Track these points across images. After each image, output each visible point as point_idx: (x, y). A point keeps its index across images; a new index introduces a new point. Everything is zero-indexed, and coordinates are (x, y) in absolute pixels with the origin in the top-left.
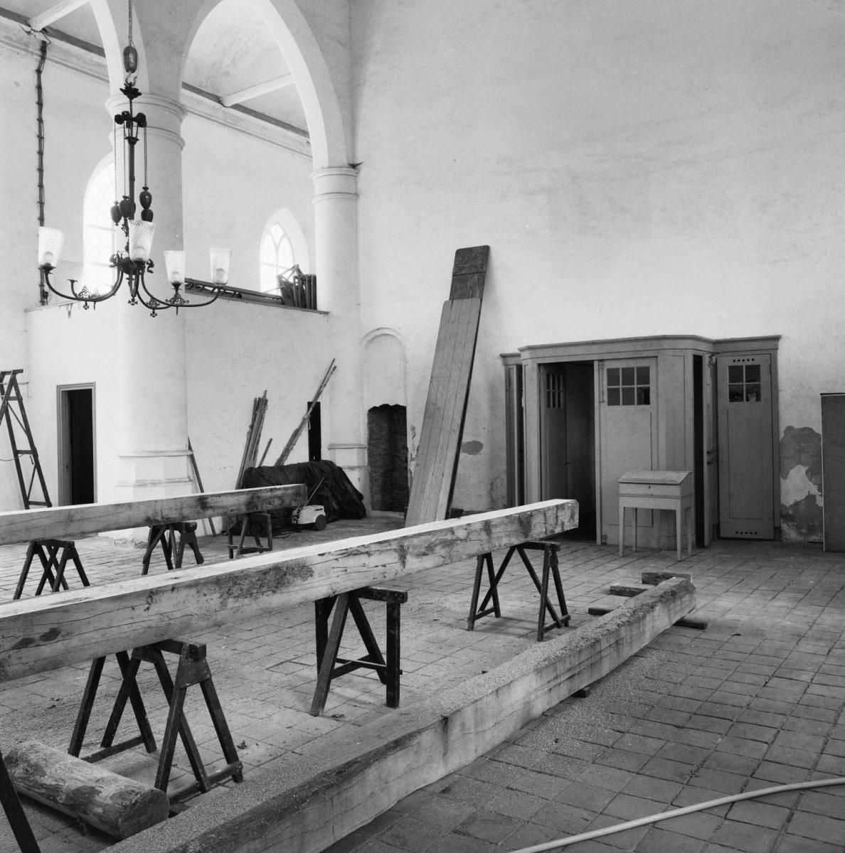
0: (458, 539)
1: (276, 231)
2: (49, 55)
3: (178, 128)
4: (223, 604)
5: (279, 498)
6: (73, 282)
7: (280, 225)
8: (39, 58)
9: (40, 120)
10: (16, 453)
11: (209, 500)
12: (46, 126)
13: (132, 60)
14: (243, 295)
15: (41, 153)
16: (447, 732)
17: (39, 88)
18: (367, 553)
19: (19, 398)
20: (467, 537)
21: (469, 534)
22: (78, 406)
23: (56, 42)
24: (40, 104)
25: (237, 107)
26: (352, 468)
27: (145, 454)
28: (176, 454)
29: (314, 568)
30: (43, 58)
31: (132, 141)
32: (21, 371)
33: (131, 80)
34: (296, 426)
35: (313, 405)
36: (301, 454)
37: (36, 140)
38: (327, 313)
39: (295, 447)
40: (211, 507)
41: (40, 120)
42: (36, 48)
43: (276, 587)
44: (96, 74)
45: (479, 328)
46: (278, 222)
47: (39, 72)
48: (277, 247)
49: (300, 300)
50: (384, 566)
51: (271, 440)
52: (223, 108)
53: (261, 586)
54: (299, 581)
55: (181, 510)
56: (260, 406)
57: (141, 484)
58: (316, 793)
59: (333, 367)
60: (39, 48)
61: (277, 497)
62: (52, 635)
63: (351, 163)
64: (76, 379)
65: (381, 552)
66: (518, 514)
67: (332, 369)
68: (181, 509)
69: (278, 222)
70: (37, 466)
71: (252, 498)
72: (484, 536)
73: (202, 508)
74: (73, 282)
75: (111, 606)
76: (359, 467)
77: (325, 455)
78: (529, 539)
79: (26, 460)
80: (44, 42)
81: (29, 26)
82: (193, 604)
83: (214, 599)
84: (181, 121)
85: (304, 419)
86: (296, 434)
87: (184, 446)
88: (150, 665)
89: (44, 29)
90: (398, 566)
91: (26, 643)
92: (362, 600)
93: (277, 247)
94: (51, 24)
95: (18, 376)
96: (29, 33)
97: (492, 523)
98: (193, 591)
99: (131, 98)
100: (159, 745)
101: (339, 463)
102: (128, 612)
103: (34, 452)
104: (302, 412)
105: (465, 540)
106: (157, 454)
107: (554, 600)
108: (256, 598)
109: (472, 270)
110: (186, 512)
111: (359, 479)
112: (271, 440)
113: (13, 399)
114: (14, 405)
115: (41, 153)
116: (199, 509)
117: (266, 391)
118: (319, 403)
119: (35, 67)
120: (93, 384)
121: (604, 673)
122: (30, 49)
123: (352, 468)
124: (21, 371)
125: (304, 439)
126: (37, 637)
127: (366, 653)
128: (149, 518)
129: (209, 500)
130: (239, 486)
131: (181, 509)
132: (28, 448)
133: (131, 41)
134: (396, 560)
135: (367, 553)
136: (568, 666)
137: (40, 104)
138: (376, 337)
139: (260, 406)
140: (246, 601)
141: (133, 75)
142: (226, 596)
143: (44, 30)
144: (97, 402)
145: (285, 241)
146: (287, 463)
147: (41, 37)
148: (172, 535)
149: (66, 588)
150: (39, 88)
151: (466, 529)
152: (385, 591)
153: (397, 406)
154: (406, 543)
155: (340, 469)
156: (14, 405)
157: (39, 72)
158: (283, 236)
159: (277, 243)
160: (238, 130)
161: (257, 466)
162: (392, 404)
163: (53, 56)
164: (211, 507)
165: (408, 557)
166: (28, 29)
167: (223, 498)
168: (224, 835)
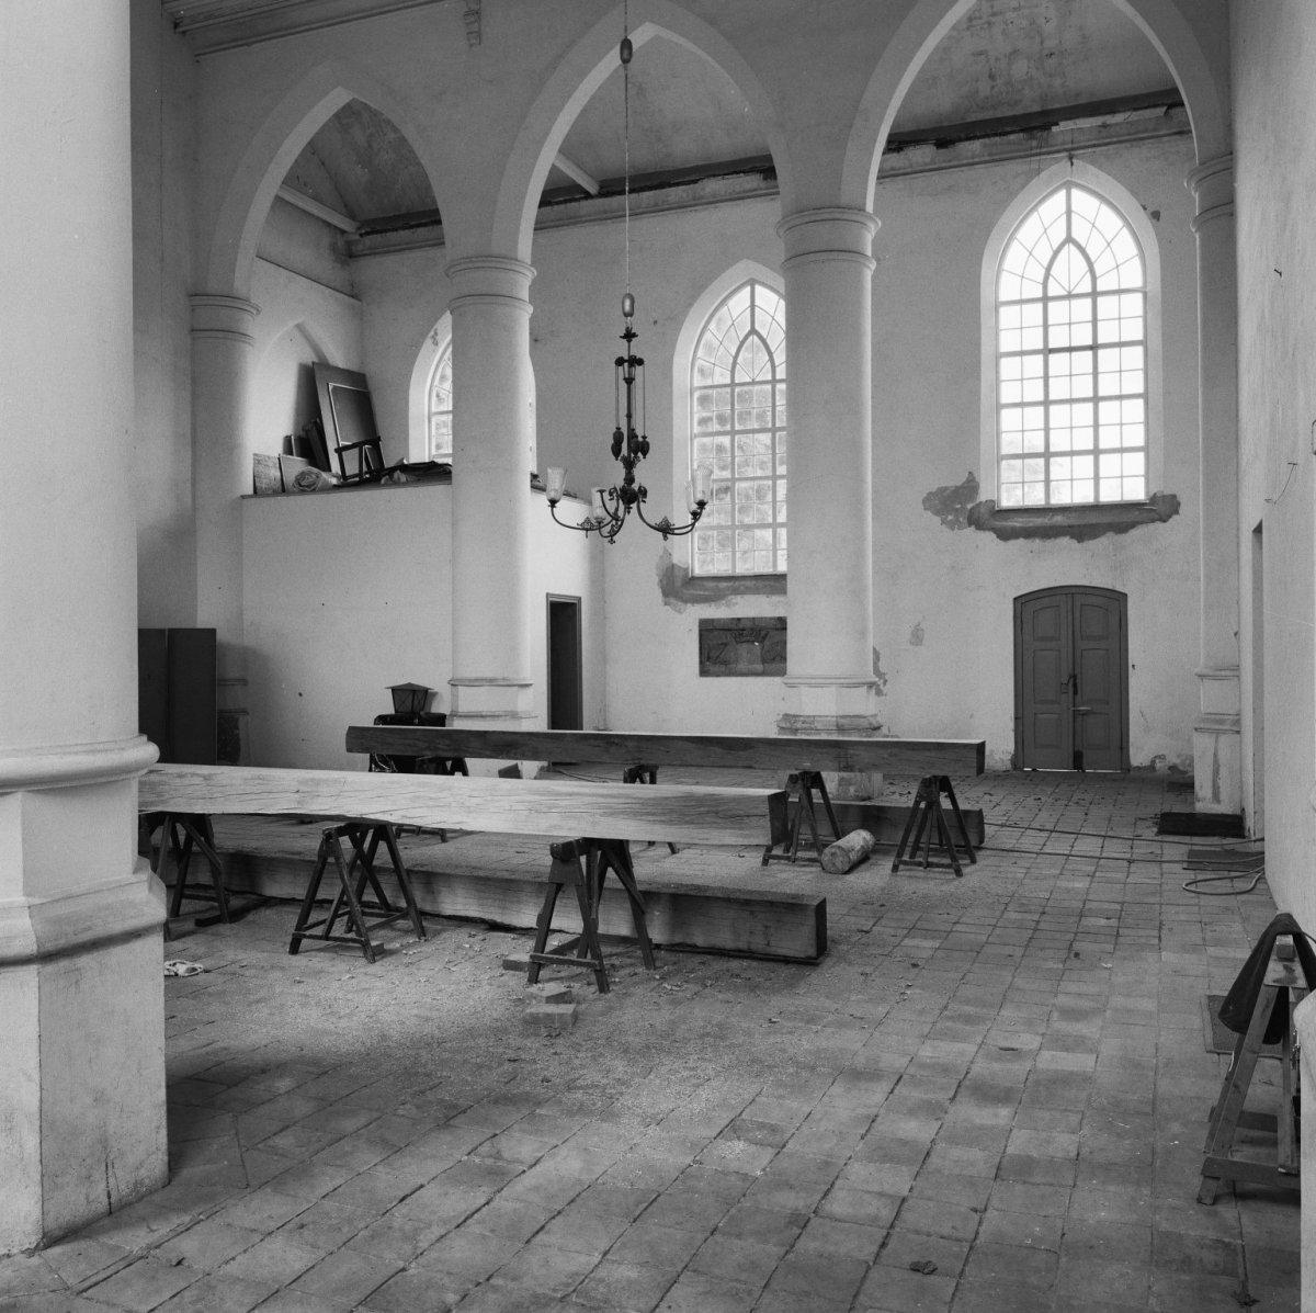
31: (629, 381)
99: (629, 341)
130: (221, 712)
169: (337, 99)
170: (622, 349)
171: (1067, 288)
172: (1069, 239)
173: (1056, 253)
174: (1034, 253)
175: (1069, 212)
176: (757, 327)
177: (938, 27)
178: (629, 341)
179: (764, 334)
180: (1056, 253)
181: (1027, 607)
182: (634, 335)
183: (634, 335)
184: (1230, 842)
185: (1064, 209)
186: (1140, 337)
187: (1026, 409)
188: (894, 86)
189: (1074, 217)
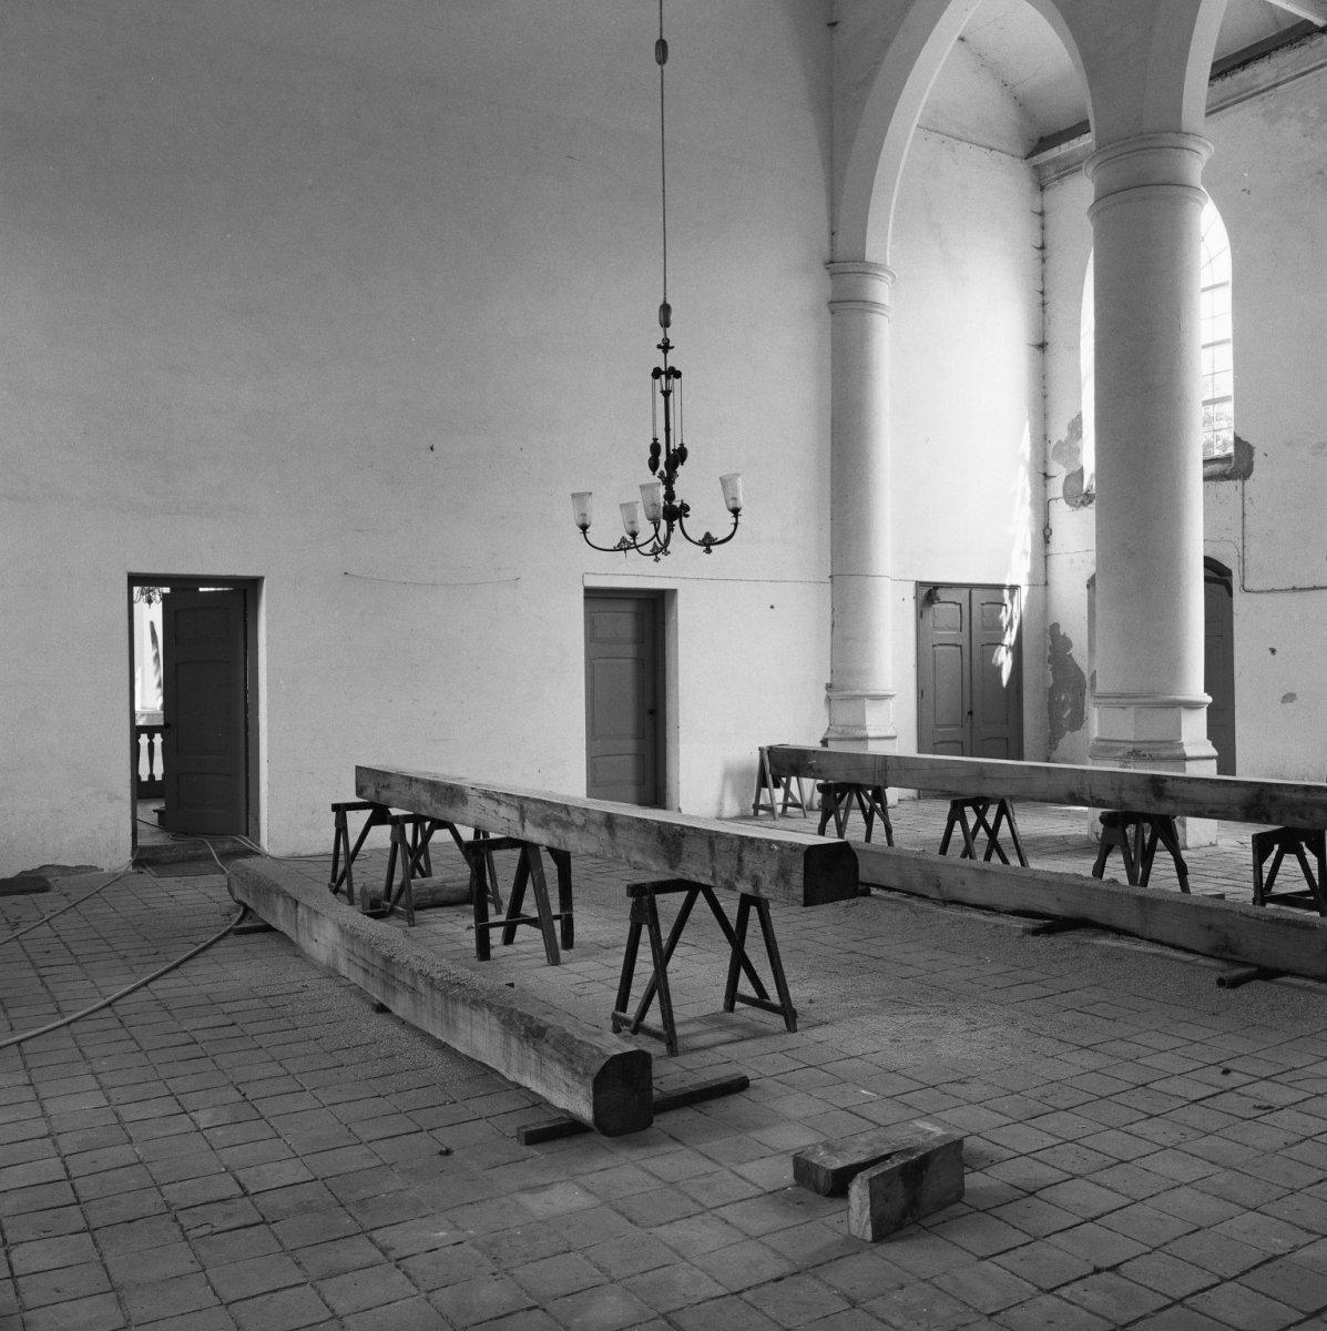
18: (497, 800)
20: (584, 826)
31: (666, 394)
44: (1215, 108)
45: (127, 673)
55: (1120, 792)
66: (658, 822)
68: (1120, 790)
71: (1258, 797)
72: (604, 834)
73: (1155, 795)
88: (755, 908)
92: (701, 894)
94: (1216, 54)
97: (617, 821)
99: (665, 352)
100: (506, 902)
107: (645, 955)
109: (211, 628)
116: (1149, 795)
128: (1073, 794)
129: (1169, 785)
135: (497, 800)
144: (681, 660)
148: (1139, 833)
149: (971, 857)
164: (1172, 798)
178: (665, 352)
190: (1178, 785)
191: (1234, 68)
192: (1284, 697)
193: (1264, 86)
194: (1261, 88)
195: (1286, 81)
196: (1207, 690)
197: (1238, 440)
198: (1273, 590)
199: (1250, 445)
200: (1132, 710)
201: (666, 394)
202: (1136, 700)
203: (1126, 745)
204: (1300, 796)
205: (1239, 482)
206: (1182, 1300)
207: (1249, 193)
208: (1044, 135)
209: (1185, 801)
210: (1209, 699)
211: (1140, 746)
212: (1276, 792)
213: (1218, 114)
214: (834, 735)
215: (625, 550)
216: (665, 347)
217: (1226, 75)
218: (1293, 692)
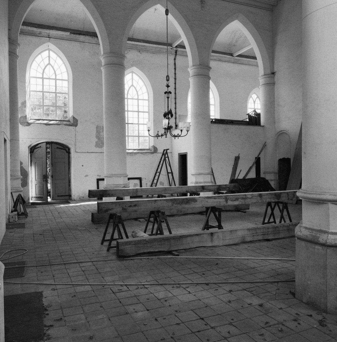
0: (248, 198)
1: (254, 96)
2: (178, 53)
3: (209, 74)
4: (172, 205)
5: (228, 187)
6: (158, 131)
7: (256, 94)
8: (175, 55)
9: (175, 74)
10: (168, 173)
11: (205, 187)
12: (177, 75)
13: (168, 79)
14: (234, 122)
15: (175, 83)
16: (212, 236)
17: (175, 64)
18: (214, 198)
19: (168, 157)
21: (252, 197)
22: (183, 158)
23: (179, 49)
24: (175, 69)
25: (240, 56)
26: (272, 180)
27: (198, 174)
28: (207, 174)
29: (197, 200)
30: (176, 55)
31: (168, 98)
32: (169, 149)
33: (168, 83)
34: (251, 165)
35: (257, 158)
36: (252, 175)
37: (174, 80)
38: (263, 126)
39: (250, 173)
40: (206, 189)
41: (175, 74)
42: (174, 52)
43: (187, 203)
46: (255, 93)
47: (175, 59)
48: (254, 102)
49: (255, 122)
50: (220, 202)
51: (241, 170)
52: (233, 57)
53: (182, 202)
54: (193, 203)
56: (237, 159)
57: (196, 183)
58: (174, 238)
59: (265, 145)
60: (175, 52)
61: (227, 187)
62: (135, 206)
63: (272, 72)
64: (183, 151)
65: (219, 198)
67: (265, 145)
69: (255, 93)
70: (173, 178)
71: (219, 187)
74: (158, 131)
75: (147, 202)
76: (274, 180)
77: (262, 175)
78: (280, 201)
79: (170, 175)
80: (176, 50)
81: (172, 46)
82: (165, 204)
83: (170, 204)
84: (210, 71)
85: (254, 163)
86: (251, 168)
87: (209, 171)
89: (176, 46)
90: (225, 203)
91: (130, 206)
93: (254, 102)
95: (168, 151)
96: (172, 49)
98: (165, 201)
99: (168, 87)
101: (267, 179)
102: (151, 203)
103: (172, 173)
104: (253, 160)
105: (251, 198)
106: (200, 174)
108: (181, 205)
110: (198, 190)
111: (274, 184)
112: (241, 170)
113: (166, 157)
114: (167, 159)
115: (175, 83)
117: (239, 154)
118: (260, 158)
119: (174, 58)
120: (187, 153)
121: (281, 237)
122: (172, 53)
123: (272, 180)
124: (169, 149)
125: (254, 170)
126: (132, 205)
127: (218, 225)
129: (205, 187)
130: (229, 183)
131: (196, 189)
132: (170, 172)
133: (168, 74)
134: (224, 201)
135: (214, 198)
136: (262, 231)
137: (175, 69)
138: (281, 134)
139: (237, 159)
140: (178, 205)
141: (168, 82)
142: (173, 203)
143: (176, 47)
145: (258, 99)
146: (246, 178)
147: (175, 49)
150: (175, 64)
151: (251, 195)
152: (218, 208)
153: (288, 158)
154: (228, 197)
155: (267, 180)
156: (167, 159)
157: (175, 59)
158: (257, 98)
159: (255, 101)
160: (240, 64)
161: (236, 178)
162: (286, 157)
163: (179, 53)
164: (206, 189)
165: (229, 201)
166: (171, 48)
167: (210, 187)
168: (153, 240)
169: (252, 47)
170: (166, 89)
171: (133, 96)
172: (132, 85)
173: (46, 67)
174: (140, 88)
175: (49, 57)
176: (51, 63)
177: (101, 19)
178: (168, 87)
179: (135, 87)
180: (46, 67)
181: (290, 159)
182: (169, 86)
183: (169, 86)
184: (7, 262)
185: (131, 78)
186: (147, 110)
187: (137, 118)
188: (150, 47)
189: (134, 80)
190: (207, 187)
191: (77, 34)
192: (85, 176)
193: (81, 41)
194: (80, 41)
195: (86, 42)
196: (21, 175)
197: (74, 118)
198: (92, 152)
199: (77, 119)
200: (122, 178)
201: (168, 98)
202: (123, 175)
203: (122, 185)
204: (225, 186)
205: (74, 127)
206: (137, 296)
207: (77, 62)
208: (211, 70)
209: (208, 189)
210: (22, 177)
211: (125, 185)
212: (221, 186)
213: (62, 40)
214: (14, 191)
215: (178, 137)
216: (168, 86)
217: (75, 34)
218: (87, 174)
